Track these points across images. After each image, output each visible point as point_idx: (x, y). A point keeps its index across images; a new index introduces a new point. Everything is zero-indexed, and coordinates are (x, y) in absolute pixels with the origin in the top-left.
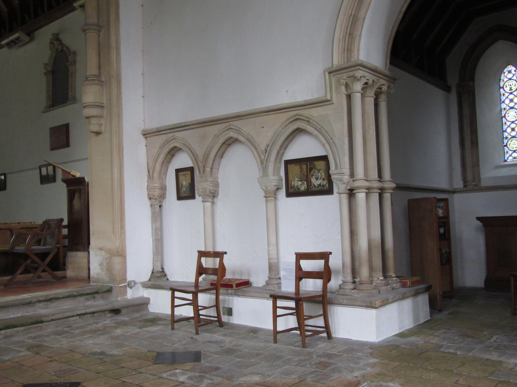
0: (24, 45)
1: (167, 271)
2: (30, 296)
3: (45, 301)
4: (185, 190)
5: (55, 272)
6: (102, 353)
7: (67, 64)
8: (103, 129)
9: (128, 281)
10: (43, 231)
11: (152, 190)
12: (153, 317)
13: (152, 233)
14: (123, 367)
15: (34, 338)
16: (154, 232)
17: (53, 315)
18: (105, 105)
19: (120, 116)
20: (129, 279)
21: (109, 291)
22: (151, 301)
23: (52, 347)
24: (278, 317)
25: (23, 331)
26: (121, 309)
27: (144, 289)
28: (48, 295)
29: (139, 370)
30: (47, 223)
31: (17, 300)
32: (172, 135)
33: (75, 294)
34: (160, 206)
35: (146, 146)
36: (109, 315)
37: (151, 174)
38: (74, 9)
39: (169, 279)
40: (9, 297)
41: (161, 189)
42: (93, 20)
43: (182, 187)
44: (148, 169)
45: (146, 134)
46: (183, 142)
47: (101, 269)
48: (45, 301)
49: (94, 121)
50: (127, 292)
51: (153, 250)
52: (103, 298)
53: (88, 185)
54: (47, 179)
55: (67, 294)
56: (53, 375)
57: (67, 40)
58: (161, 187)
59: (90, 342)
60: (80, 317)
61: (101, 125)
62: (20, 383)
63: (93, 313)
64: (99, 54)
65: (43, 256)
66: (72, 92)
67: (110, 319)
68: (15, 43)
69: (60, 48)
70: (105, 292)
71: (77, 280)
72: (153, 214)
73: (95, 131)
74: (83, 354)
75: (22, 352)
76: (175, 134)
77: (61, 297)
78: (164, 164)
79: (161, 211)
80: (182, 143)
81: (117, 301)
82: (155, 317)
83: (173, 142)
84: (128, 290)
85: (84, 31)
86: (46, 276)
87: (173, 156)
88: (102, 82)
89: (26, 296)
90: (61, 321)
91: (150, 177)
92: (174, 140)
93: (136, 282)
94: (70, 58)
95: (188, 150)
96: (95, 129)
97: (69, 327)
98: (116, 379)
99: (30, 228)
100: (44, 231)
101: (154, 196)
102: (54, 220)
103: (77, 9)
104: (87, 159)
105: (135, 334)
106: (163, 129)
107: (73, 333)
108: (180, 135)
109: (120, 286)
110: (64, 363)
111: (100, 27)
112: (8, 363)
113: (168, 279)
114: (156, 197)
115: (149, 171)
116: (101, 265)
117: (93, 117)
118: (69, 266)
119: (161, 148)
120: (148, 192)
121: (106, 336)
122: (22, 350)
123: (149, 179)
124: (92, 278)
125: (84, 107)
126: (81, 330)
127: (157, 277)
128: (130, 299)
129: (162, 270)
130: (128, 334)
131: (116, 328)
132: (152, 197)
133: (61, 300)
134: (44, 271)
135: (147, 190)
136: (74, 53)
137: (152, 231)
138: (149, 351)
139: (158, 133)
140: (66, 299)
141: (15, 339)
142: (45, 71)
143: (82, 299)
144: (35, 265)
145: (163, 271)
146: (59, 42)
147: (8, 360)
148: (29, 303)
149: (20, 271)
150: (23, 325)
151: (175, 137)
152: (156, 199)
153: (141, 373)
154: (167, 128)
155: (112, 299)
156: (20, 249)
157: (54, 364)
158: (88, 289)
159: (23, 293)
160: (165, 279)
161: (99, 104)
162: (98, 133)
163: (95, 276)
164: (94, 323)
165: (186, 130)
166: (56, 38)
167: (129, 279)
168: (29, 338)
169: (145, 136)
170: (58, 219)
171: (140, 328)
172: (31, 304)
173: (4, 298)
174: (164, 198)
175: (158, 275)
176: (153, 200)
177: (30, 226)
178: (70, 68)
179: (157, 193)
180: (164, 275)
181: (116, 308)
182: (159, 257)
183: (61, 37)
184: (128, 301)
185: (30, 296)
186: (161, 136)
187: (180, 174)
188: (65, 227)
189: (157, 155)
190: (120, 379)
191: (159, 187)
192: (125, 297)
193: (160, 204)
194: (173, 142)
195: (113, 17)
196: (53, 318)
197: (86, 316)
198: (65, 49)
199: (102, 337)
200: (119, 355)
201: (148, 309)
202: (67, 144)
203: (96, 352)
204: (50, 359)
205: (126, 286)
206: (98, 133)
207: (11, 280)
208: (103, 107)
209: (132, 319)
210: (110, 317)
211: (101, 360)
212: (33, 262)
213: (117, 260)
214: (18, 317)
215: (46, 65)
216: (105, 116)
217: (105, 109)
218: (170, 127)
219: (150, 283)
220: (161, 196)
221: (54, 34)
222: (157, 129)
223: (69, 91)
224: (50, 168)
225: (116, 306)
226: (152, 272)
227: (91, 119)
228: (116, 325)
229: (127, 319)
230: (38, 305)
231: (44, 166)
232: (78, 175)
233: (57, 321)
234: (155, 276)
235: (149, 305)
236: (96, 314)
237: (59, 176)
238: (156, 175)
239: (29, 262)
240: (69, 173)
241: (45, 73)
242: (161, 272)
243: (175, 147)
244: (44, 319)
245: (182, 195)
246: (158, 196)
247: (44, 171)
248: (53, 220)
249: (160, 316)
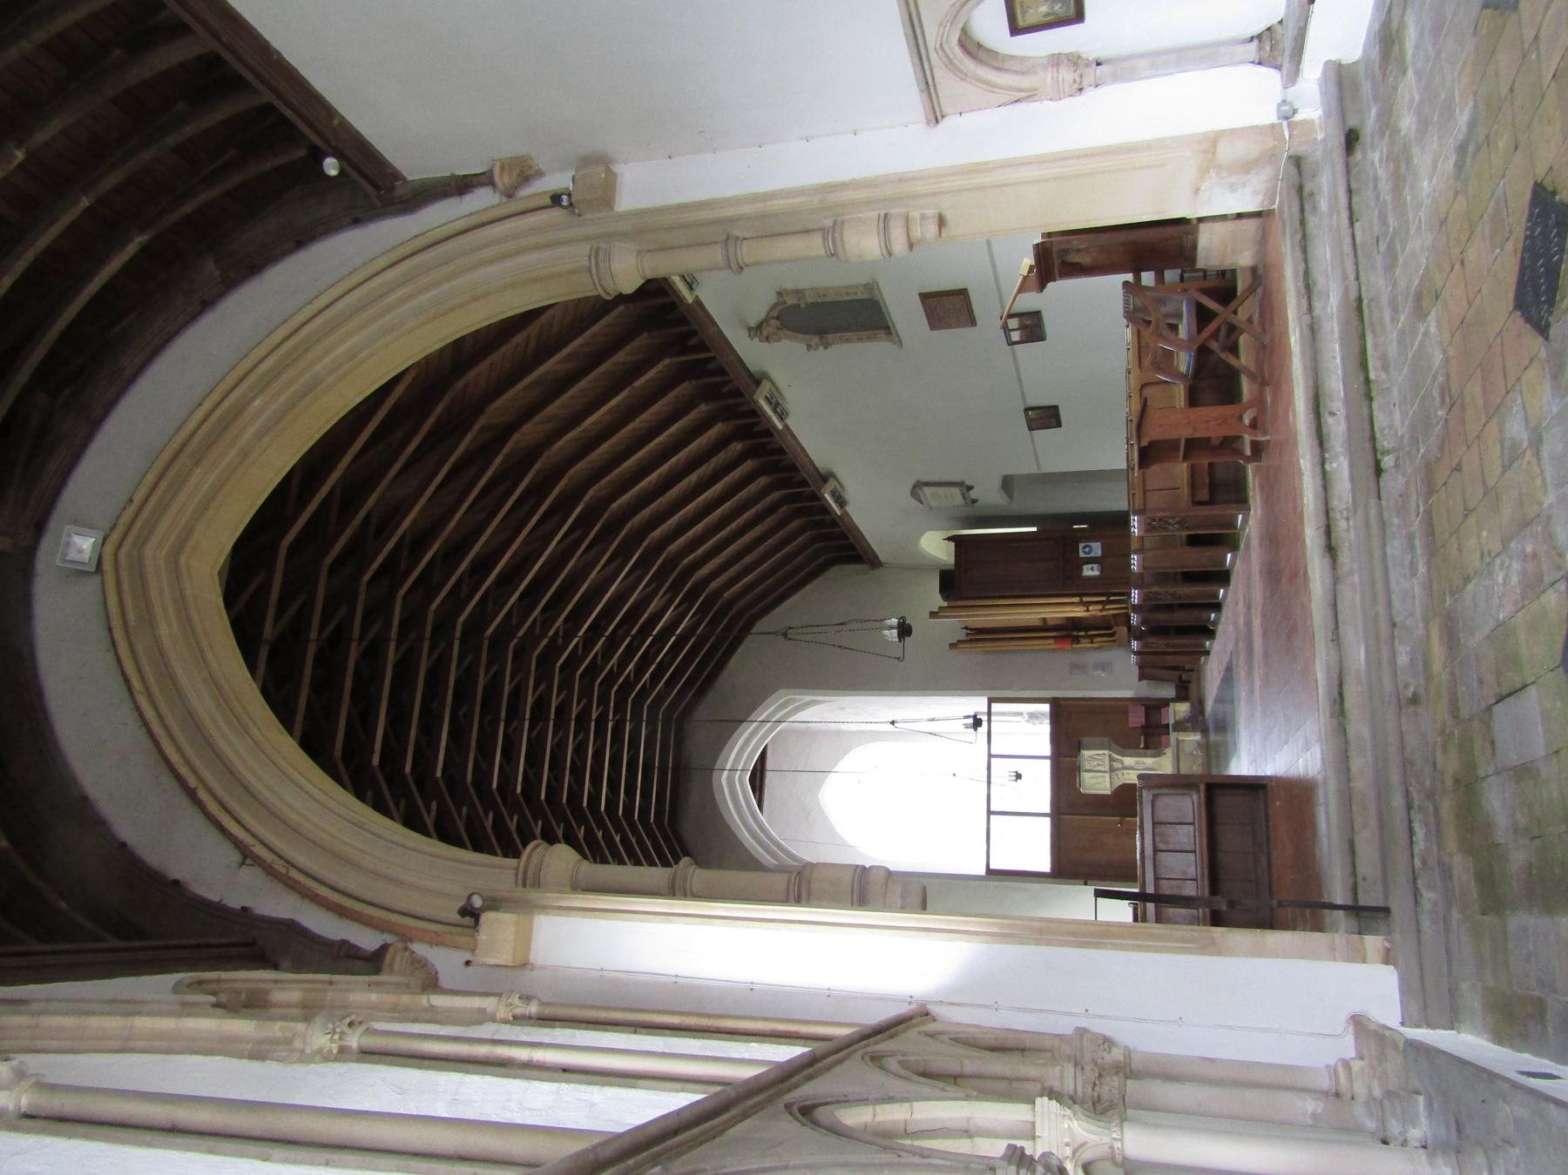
0: (777, 389)
1: (1256, 30)
2: (1294, 330)
3: (1309, 299)
4: (1060, 5)
5: (1239, 294)
6: (1462, 149)
7: (803, 306)
8: (931, 212)
9: (1279, 118)
10: (1149, 323)
11: (1061, 87)
12: (1378, 46)
13: (1163, 75)
14: (1511, 90)
15: (1395, 310)
16: (1159, 72)
17: (1345, 278)
18: (882, 213)
19: (901, 179)
20: (1272, 118)
21: (1297, 161)
22: (1333, 57)
23: (1427, 268)
24: (956, 546)
25: (1375, 336)
26: (1347, 129)
27: (1300, 79)
28: (1298, 293)
29: (1526, 46)
30: (1132, 315)
31: (1303, 354)
32: (933, 55)
33: (1299, 236)
34: (1098, 64)
35: (961, 114)
36: (1358, 156)
37: (1022, 95)
38: (698, 302)
39: (1280, 19)
40: (1294, 371)
41: (1058, 65)
42: (716, 254)
43: (1054, 13)
44: (1012, 103)
45: (936, 116)
46: (948, 24)
47: (1244, 185)
48: (1309, 299)
49: (917, 232)
50: (1305, 120)
51: (1204, 69)
52: (1314, 176)
53: (1049, 235)
54: (1032, 327)
55: (1299, 254)
56: (1502, 250)
57: (757, 313)
58: (1053, 66)
59: (1426, 184)
60: (1357, 221)
61: (923, 217)
62: (1509, 317)
63: (1350, 192)
64: (781, 234)
65: (1203, 316)
66: (856, 293)
67: (1369, 151)
68: (777, 404)
69: (775, 323)
70: (1299, 172)
71: (1263, 240)
72: (1116, 78)
73: (937, 230)
74: (1457, 193)
75: (1427, 329)
76: (931, 46)
77: (1304, 266)
78: (1000, 65)
79: (1109, 61)
80: (952, 24)
81: (1324, 140)
82: (1377, 41)
83: (949, 48)
84: (1298, 118)
85: (742, 268)
86: (1246, 311)
87: (980, 46)
88: (835, 222)
89: (1295, 339)
90: (1362, 262)
91: (1030, 95)
92: (946, 47)
93: (1280, 101)
94: (791, 301)
95: (965, 8)
96: (932, 228)
97: (1378, 241)
98: (1543, 98)
99: (1140, 349)
100: (1150, 319)
101: (1074, 81)
102: (1125, 300)
103: (697, 296)
105: (1419, 79)
106: (920, 76)
107: (1394, 229)
108: (932, 34)
109: (1287, 138)
110: (1472, 233)
111: (727, 239)
112: (1451, 352)
113: (1281, 22)
114: (1077, 76)
115: (1016, 101)
116: (1233, 188)
117: (908, 235)
118: (1227, 263)
119: (964, 77)
120: (1064, 97)
121: (1416, 150)
122: (1422, 330)
123: (1037, 98)
124: (1262, 205)
125: (890, 254)
126: (1390, 214)
127: (1271, 50)
128: (1324, 111)
129: (1256, 41)
130: (1417, 97)
131: (1395, 131)
132: (1076, 86)
133: (1310, 265)
134: (1235, 312)
135: (1060, 99)
136: (780, 294)
137: (1157, 76)
138: (1475, 33)
139: (932, 88)
140: (1309, 256)
141: (1392, 351)
142: (821, 348)
143: (1312, 221)
144: (1223, 331)
145: (1259, 37)
146: (764, 324)
147: (1444, 352)
148: (1313, 331)
149: (1232, 361)
150: (1363, 337)
151: (938, 46)
152: (1081, 76)
153: (1536, 38)
154: (918, 68)
155: (1319, 153)
156: (1184, 362)
157: (1472, 255)
158: (1291, 212)
159: (1288, 346)
160: (1279, 29)
161: (882, 225)
162: (941, 222)
163: (1259, 198)
164: (1375, 187)
165: (920, 20)
166: (756, 330)
167: (1272, 118)
168: (1394, 320)
169: (939, 118)
170: (1124, 292)
171: (1404, 72)
172: (1315, 327)
173: (1295, 380)
174: (1079, 57)
175: (1268, 48)
176: (1085, 83)
177: (1137, 350)
178: (810, 300)
179: (1067, 75)
180: (1268, 32)
181: (1343, 139)
182: (1222, 50)
183: (753, 323)
184: (1327, 114)
185: (1294, 330)
186: (937, 81)
187: (1021, 23)
188: (1138, 278)
189: (980, 85)
190: (1545, 87)
191: (1053, 72)
192: (1317, 123)
193: (1094, 65)
194: (949, 48)
195: (705, 215)
196: (1352, 277)
197: (1355, 207)
198: (775, 313)
199: (1416, 161)
200: (1475, 107)
201: (1353, 63)
202: (963, 293)
203: (1455, 165)
204: (1457, 267)
205: (1290, 126)
206: (941, 222)
207: (1252, 377)
208: (886, 215)
209: (1375, 98)
210: (1364, 152)
211: (1478, 149)
212: (1215, 335)
213: (1226, 153)
214: (1342, 349)
215: (809, 347)
216: (904, 210)
217: (891, 211)
218: (918, 62)
219: (1286, 66)
220: (1076, 64)
221: (749, 336)
222: (922, 91)
223: (856, 298)
224: (1013, 323)
225: (1338, 140)
226: (1259, 63)
227: (913, 239)
228: (1388, 133)
229: (1374, 111)
230: (1317, 312)
231: (1008, 337)
232: (1029, 261)
233: (1360, 268)
234: (1269, 57)
235: (1343, 62)
236: (1354, 186)
237: (1029, 301)
238: (1025, 82)
239: (1214, 345)
240: (1025, 278)
241: (826, 348)
242: (1260, 41)
243: (961, 44)
244: (1353, 295)
245: (1072, 11)
246: (1075, 71)
247: (1015, 336)
248: (1126, 302)
249: (1377, 27)
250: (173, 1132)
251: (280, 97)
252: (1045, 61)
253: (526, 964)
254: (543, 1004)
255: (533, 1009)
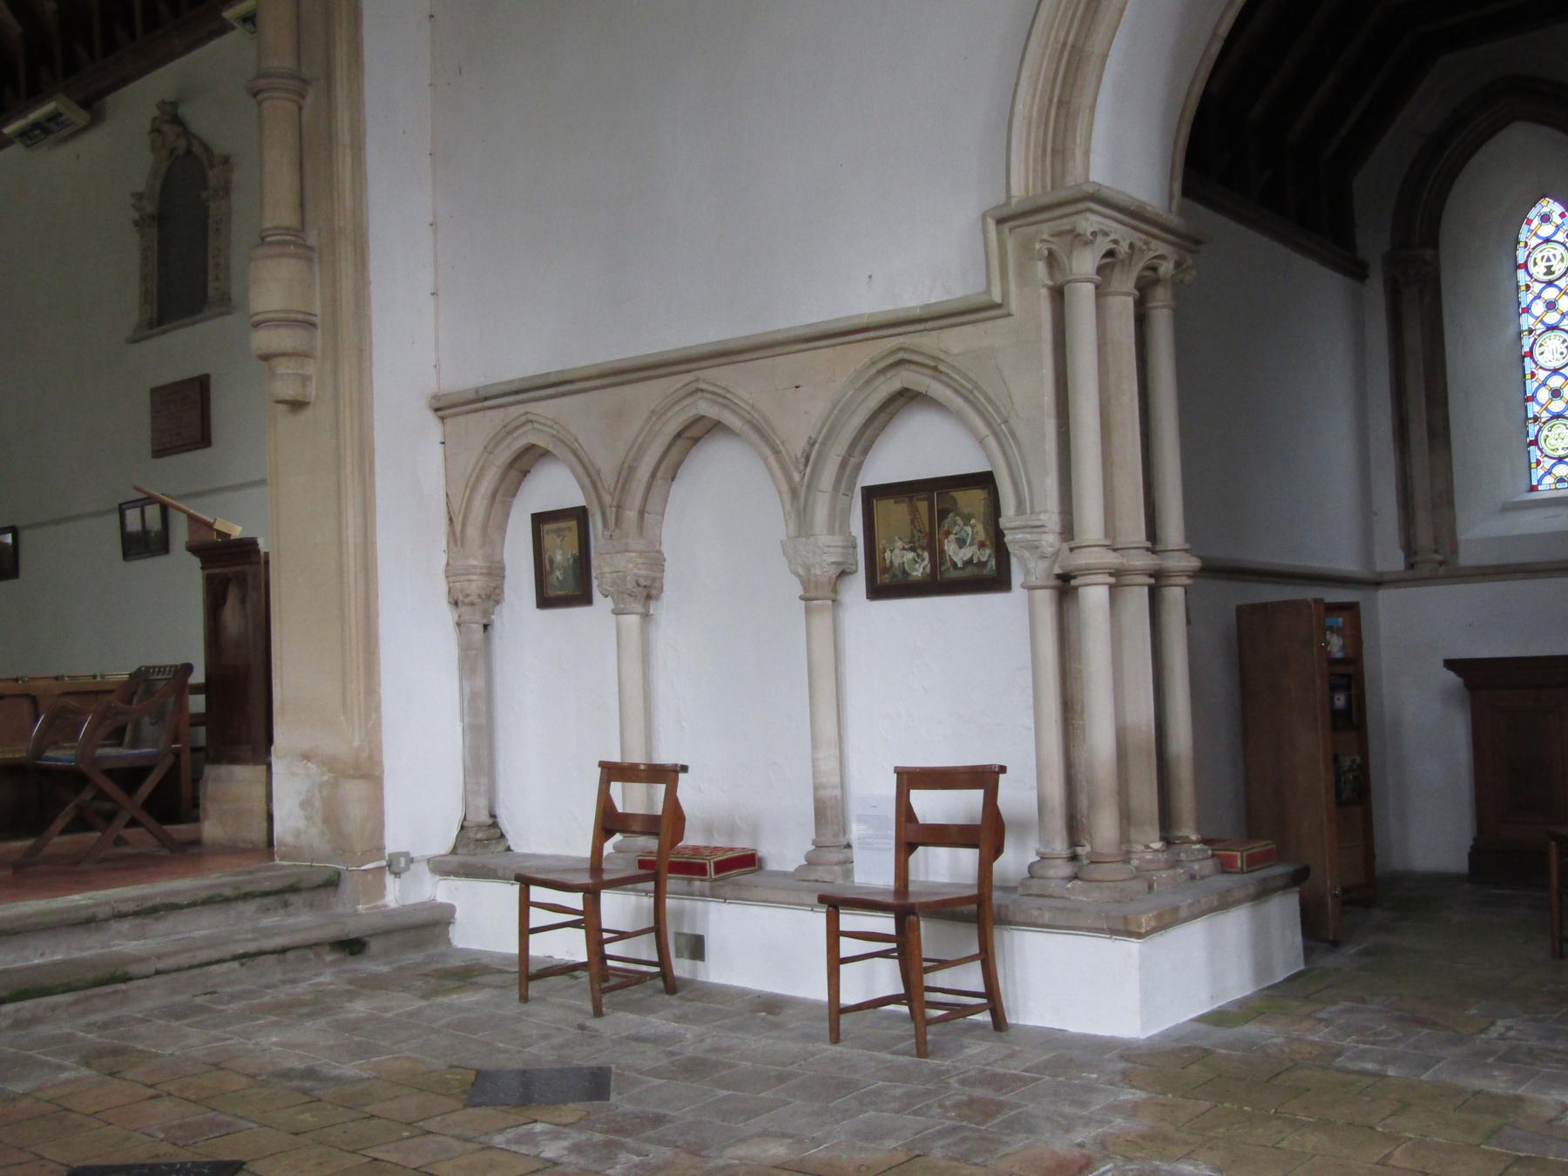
0: (73, 135)
1: (505, 823)
2: (90, 898)
3: (136, 914)
4: (561, 578)
5: (166, 827)
6: (310, 1073)
7: (204, 195)
8: (312, 391)
9: (390, 855)
10: (129, 702)
11: (462, 578)
12: (463, 964)
13: (462, 709)
14: (372, 1116)
15: (104, 1026)
16: (466, 704)
17: (160, 957)
18: (317, 320)
19: (363, 352)
20: (391, 846)
21: (332, 883)
22: (458, 915)
23: (156, 1056)
25: (70, 1005)
26: (366, 939)
27: (438, 877)
28: (145, 898)
29: (421, 1124)
30: (141, 677)
31: (53, 912)
32: (521, 409)
33: (228, 892)
34: (486, 627)
35: (443, 443)
36: (330, 958)
37: (458, 528)
38: (224, 28)
39: (512, 848)
40: (27, 902)
41: (489, 574)
42: (282, 60)
43: (552, 569)
44: (449, 513)
45: (443, 408)
46: (555, 432)
47: (307, 818)
48: (136, 914)
49: (284, 367)
50: (385, 888)
51: (464, 761)
52: (311, 906)
53: (267, 563)
54: (141, 545)
55: (203, 895)
56: (162, 1140)
57: (203, 120)
58: (490, 568)
59: (274, 1039)
60: (242, 965)
61: (305, 379)
62: (62, 1164)
63: (283, 951)
64: (301, 165)
65: (131, 777)
66: (217, 279)
67: (333, 969)
68: (47, 132)
69: (182, 145)
70: (319, 887)
71: (233, 850)
72: (466, 649)
73: (287, 398)
74: (253, 1076)
75: (66, 1069)
76: (530, 407)
77: (185, 902)
78: (499, 497)
79: (487, 641)
80: (553, 436)
81: (356, 914)
82: (469, 963)
83: (526, 432)
84: (390, 880)
85: (255, 95)
86: (140, 839)
87: (525, 473)
88: (311, 249)
89: (78, 900)
90: (184, 976)
91: (456, 537)
92: (529, 427)
93: (412, 855)
94: (213, 176)
95: (570, 456)
96: (289, 391)
97: (211, 993)
98: (353, 1152)
99: (91, 693)
100: (135, 702)
101: (468, 595)
102: (165, 667)
103: (233, 28)
104: (263, 482)
105: (410, 1015)
106: (495, 391)
107: (223, 1011)
108: (545, 409)
109: (363, 868)
110: (195, 1102)
111: (304, 81)
112: (24, 1103)
113: (509, 849)
114: (473, 598)
115: (451, 520)
116: (305, 804)
117: (283, 355)
118: (210, 808)
119: (489, 449)
120: (449, 582)
121: (322, 1022)
122: (67, 1063)
123: (452, 545)
124: (280, 844)
125: (256, 325)
126: (245, 1003)
127: (477, 840)
128: (394, 910)
129: (490, 821)
130: (389, 1015)
131: (351, 996)
132: (461, 598)
133: (186, 911)
134: (133, 823)
135: (447, 577)
136: (226, 160)
137: (462, 701)
138: (451, 1067)
139: (479, 405)
140: (199, 908)
141: (45, 1030)
142: (136, 216)
143: (249, 908)
144: (107, 806)
145: (495, 825)
146: (180, 129)
147: (25, 1095)
148: (88, 922)
149: (60, 823)
150: (68, 988)
151: (531, 417)
152: (472, 604)
153: (429, 1132)
154: (506, 388)
155: (340, 909)
156: (62, 755)
157: (163, 1106)
158: (266, 877)
159: (71, 891)
160: (500, 848)
161: (300, 317)
162: (297, 405)
163: (289, 839)
164: (284, 982)
165: (564, 394)
166: (171, 115)
167: (391, 846)
168: (89, 1027)
169: (441, 413)
170: (177, 666)
171: (424, 997)
172: (93, 925)
173: (13, 904)
174: (498, 602)
175: (479, 836)
176: (463, 609)
177: (90, 688)
178: (213, 206)
179: (476, 585)
180: (498, 835)
181: (352, 936)
182: (484, 780)
183: (184, 111)
184: (389, 914)
185: (90, 898)
186: (489, 413)
187: (547, 527)
188: (196, 689)
189: (476, 472)
190: (363, 1152)
191: (481, 568)
192: (380, 903)
193: (485, 621)
194: (526, 432)
195: (341, 52)
196: (161, 965)
197: (261, 959)
198: (196, 149)
199: (308, 1024)
200: (361, 1080)
201: (449, 940)
202: (203, 439)
203: (291, 1070)
204: (151, 1092)
205: (382, 868)
206: (297, 405)
207: (32, 851)
208: (313, 325)
209: (401, 968)
210: (333, 963)
211: (305, 1093)
212: (100, 795)
213: (354, 790)
214: (55, 964)
215: (140, 196)
216: (318, 354)
217: (319, 332)
218: (515, 387)
219: (455, 859)
220: (488, 597)
221: (164, 102)
222: (477, 391)
223: (211, 278)
224: (153, 512)
225: (352, 929)
226: (462, 827)
227: (276, 361)
228: (352, 987)
229: (384, 969)
230: (116, 926)
231: (133, 504)
232: (237, 532)
233: (174, 975)
234: (469, 838)
235: (451, 928)
236: (290, 955)
237: (180, 534)
238: (473, 532)
239: (87, 795)
240: (210, 526)
241: (136, 223)
242: (490, 826)
243: (531, 448)
244: (134, 969)
245: (552, 592)
246: (479, 596)
247: (133, 520)
248: (161, 669)
249: (485, 961)
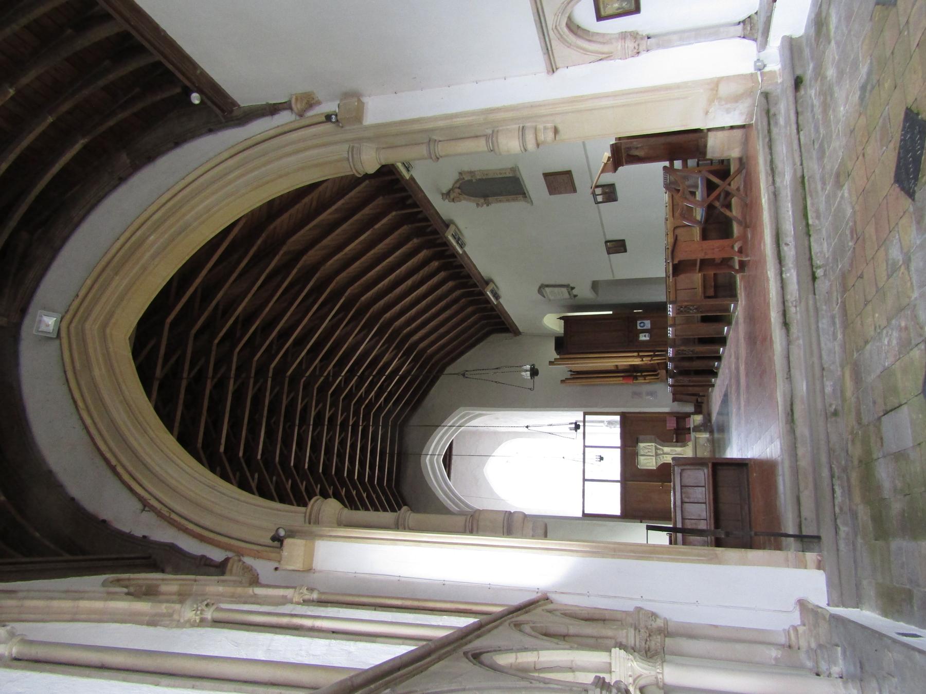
0: (459, 230)
1: (742, 18)
2: (764, 195)
3: (773, 177)
4: (626, 3)
5: (731, 174)
6: (863, 88)
7: (474, 181)
8: (550, 125)
9: (755, 70)
10: (678, 191)
11: (627, 51)
12: (814, 27)
13: (687, 44)
14: (893, 53)
15: (824, 183)
16: (685, 43)
17: (794, 164)
18: (521, 126)
19: (532, 106)
20: (751, 70)
21: (766, 95)
22: (787, 34)
23: (843, 158)
25: (812, 199)
26: (795, 76)
27: (768, 46)
28: (767, 173)
29: (901, 27)
30: (668, 186)
31: (770, 209)
32: (551, 33)
33: (767, 140)
34: (649, 38)
35: (567, 67)
36: (802, 92)
37: (604, 56)
38: (412, 178)
39: (756, 11)
40: (764, 219)
41: (625, 38)
42: (423, 150)
43: (622, 8)
44: (598, 61)
45: (552, 69)
46: (560, 14)
47: (735, 110)
48: (773, 177)
49: (541, 137)
50: (771, 71)
51: (711, 41)
52: (776, 104)
53: (620, 139)
54: (609, 193)
55: (767, 150)
56: (887, 148)
57: (447, 185)
58: (622, 39)
59: (842, 108)
60: (801, 130)
61: (545, 128)
62: (891, 187)
63: (797, 113)
64: (461, 138)
65: (710, 187)
66: (505, 173)
67: (808, 89)
68: (459, 239)
69: (458, 191)
70: (767, 101)
71: (746, 142)
72: (659, 46)
73: (553, 136)
74: (860, 114)
75: (843, 195)
76: (550, 27)
77: (770, 157)
78: (591, 39)
79: (655, 36)
80: (562, 14)
81: (782, 83)
82: (813, 24)
83: (561, 28)
84: (766, 69)
85: (438, 158)
86: (736, 183)
87: (578, 27)
88: (493, 131)
89: (765, 201)
90: (805, 155)
91: (608, 56)
92: (559, 28)
93: (756, 60)
94: (467, 178)
95: (570, 5)
96: (551, 135)
97: (814, 142)
98: (911, 58)
99: (674, 206)
100: (679, 188)
101: (635, 48)
102: (664, 177)
103: (411, 175)
104: (584, 143)
105: (838, 47)
106: (544, 45)
107: (823, 135)
108: (550, 20)
109: (760, 82)
110: (869, 138)
111: (430, 141)
112: (857, 208)
113: (756, 13)
114: (636, 45)
115: (600, 60)
116: (728, 111)
117: (536, 139)
118: (725, 156)
119: (569, 45)
120: (629, 58)
121: (836, 89)
122: (840, 195)
123: (612, 58)
124: (745, 121)
125: (526, 150)
126: (821, 126)
127: (751, 30)
128: (782, 65)
129: (742, 24)
130: (837, 57)
131: (824, 77)
132: (636, 51)
133: (773, 157)
134: (729, 184)
135: (626, 58)
136: (460, 173)
137: (683, 45)
138: (871, 20)
139: (550, 52)
140: (773, 151)
141: (822, 207)
142: (485, 205)
143: (775, 131)
144: (722, 195)
145: (744, 22)
146: (451, 191)
147: (853, 208)
148: (775, 196)
149: (728, 213)
150: (805, 199)
151: (554, 27)
152: (638, 45)
153: (907, 22)
154: (542, 40)
155: (779, 91)
156: (699, 214)
157: (869, 151)
158: (762, 125)
159: (760, 204)
160: (755, 17)
161: (521, 133)
162: (556, 131)
163: (744, 117)
164: (812, 111)
165: (543, 12)
166: (447, 195)
167: (751, 70)
168: (823, 189)
169: (555, 69)
170: (664, 173)
171: (829, 42)
172: (776, 193)
173: (765, 225)
174: (637, 34)
175: (749, 28)
176: (641, 49)
177: (671, 207)
178: (478, 177)
179: (630, 44)
180: (749, 19)
181: (793, 82)
182: (722, 29)
183: (444, 191)
184: (784, 68)
185: (764, 195)
186: (553, 48)
187: (603, 14)
188: (672, 164)
189: (579, 50)
190: (912, 51)
191: (622, 43)
192: (778, 72)
193: (646, 38)
194: (561, 28)
195: (417, 127)
196: (799, 164)
197: (800, 122)
198: (458, 185)
199: (836, 95)
200: (871, 63)
201: (799, 37)
202: (568, 173)
203: (859, 97)
204: (861, 158)
205: (762, 74)
206: (556, 131)
207: (740, 223)
208: (523, 127)
209: (812, 58)
210: (806, 90)
211: (873, 88)
212: (717, 198)
213: (724, 90)
214: (792, 206)
215: (478, 205)
216: (534, 124)
217: (526, 125)
218: (542, 37)
219: (759, 39)
220: (635, 38)
221: (443, 198)
222: (544, 54)
223: (506, 176)
224: (598, 191)
225: (790, 83)
226: (744, 37)
227: (539, 141)
228: (819, 79)
229: (811, 66)
230: (778, 184)
231: (595, 199)
232: (607, 154)
233: (803, 159)
234: (749, 33)
235: (793, 37)
236: (800, 110)
237: (608, 178)
238: (605, 48)
239: (717, 204)
240: (605, 164)
241: (488, 205)
242: (744, 24)
243: (568, 26)
244: (799, 174)
245: (633, 7)
246: (635, 42)
247: (600, 199)
248: (665, 179)
249: (813, 16)
250: (102, 669)
251: (166, 57)
252: (617, 36)
253: (310, 569)
254: (321, 593)
255: (315, 596)
